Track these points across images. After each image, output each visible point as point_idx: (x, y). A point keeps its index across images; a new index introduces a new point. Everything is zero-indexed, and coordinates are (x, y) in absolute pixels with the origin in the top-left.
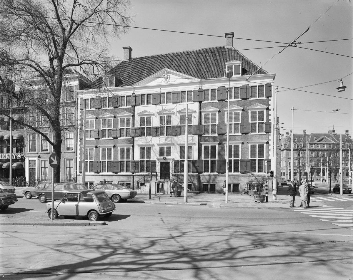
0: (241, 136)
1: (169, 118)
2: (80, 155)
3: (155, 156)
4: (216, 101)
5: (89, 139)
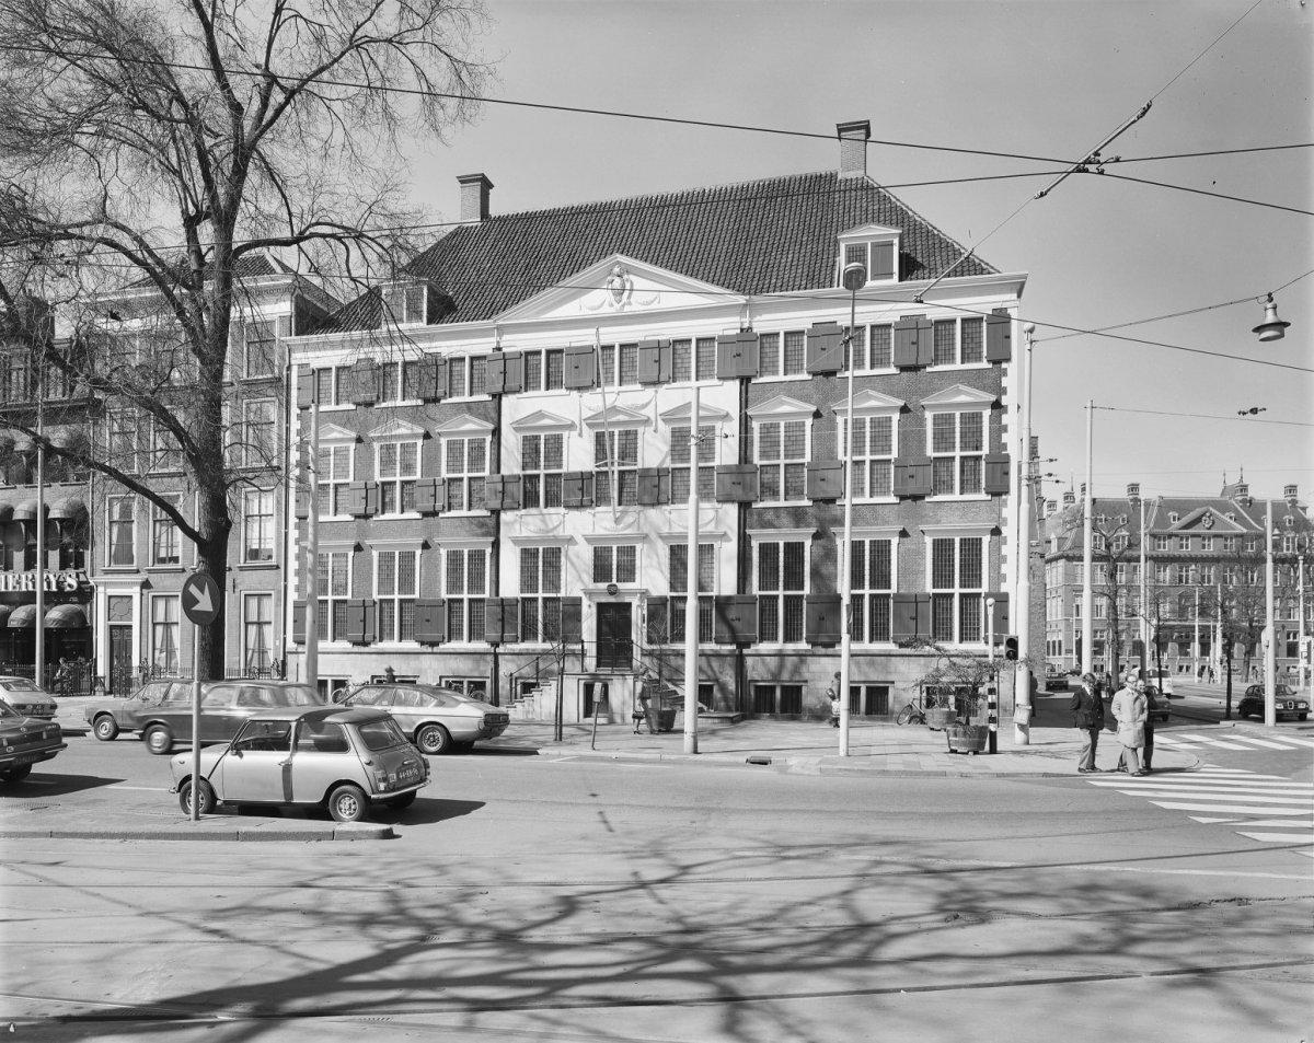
0: (896, 507)
1: (630, 438)
2: (297, 579)
3: (576, 581)
4: (805, 376)
5: (330, 518)
